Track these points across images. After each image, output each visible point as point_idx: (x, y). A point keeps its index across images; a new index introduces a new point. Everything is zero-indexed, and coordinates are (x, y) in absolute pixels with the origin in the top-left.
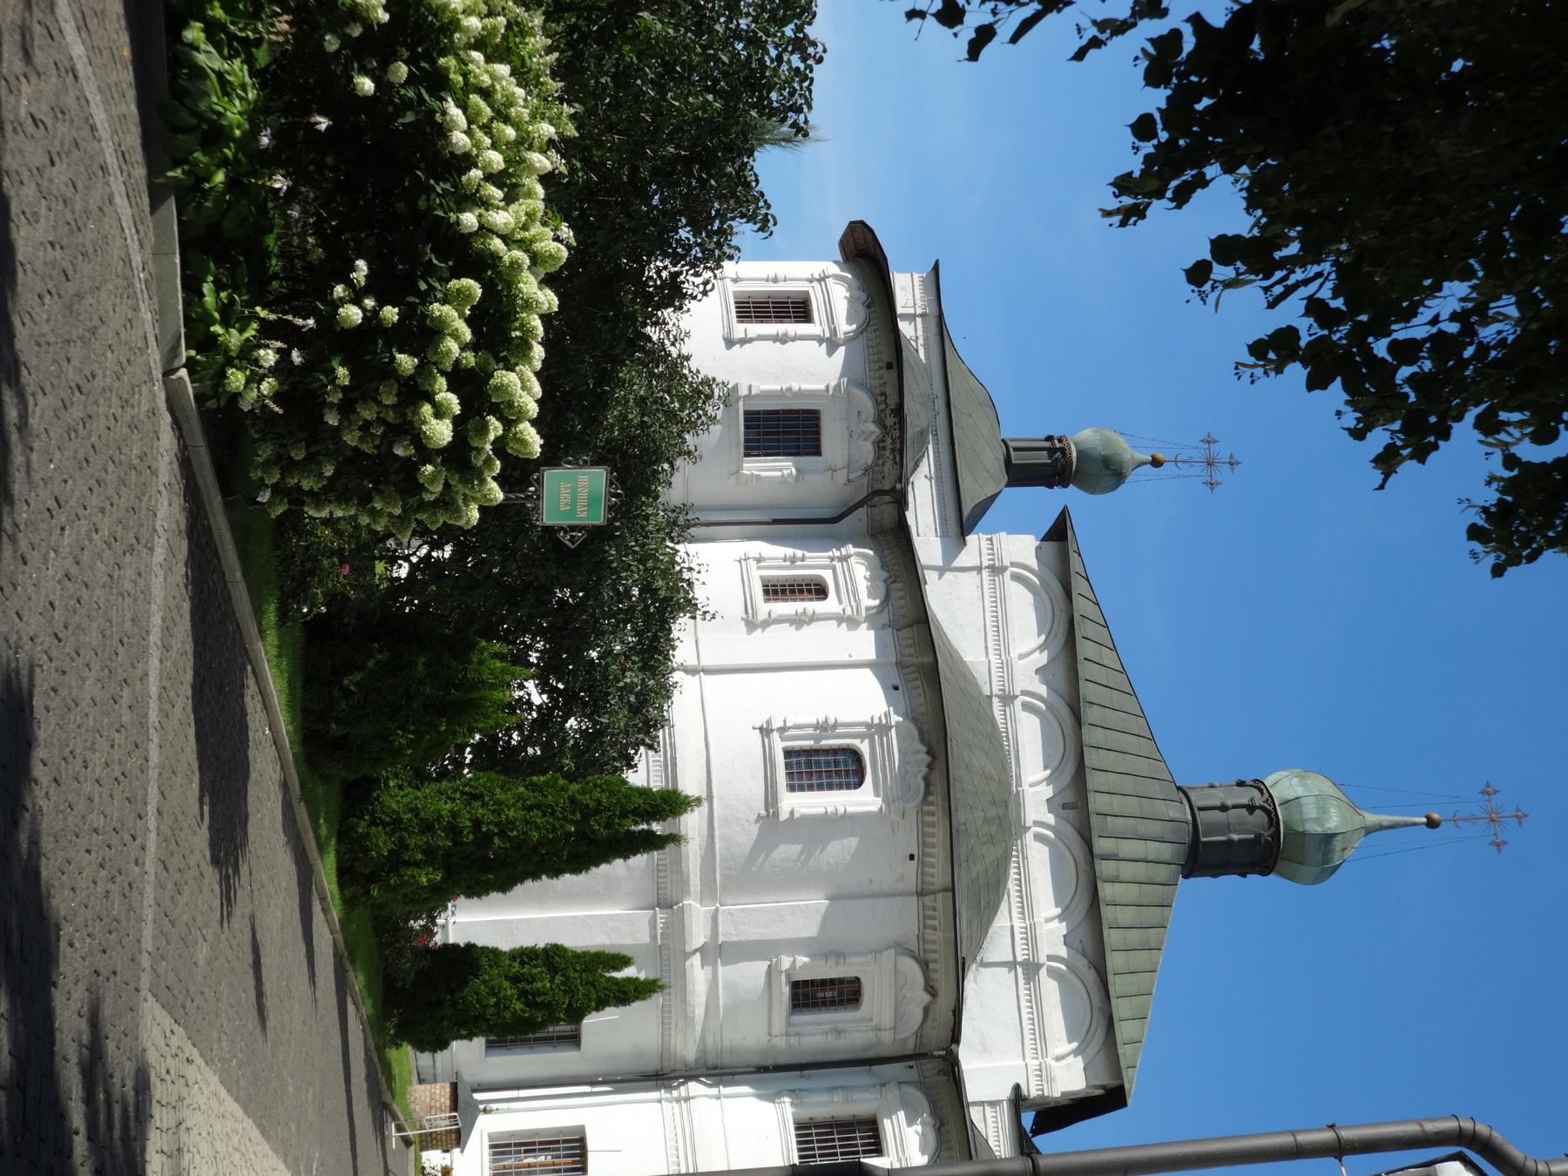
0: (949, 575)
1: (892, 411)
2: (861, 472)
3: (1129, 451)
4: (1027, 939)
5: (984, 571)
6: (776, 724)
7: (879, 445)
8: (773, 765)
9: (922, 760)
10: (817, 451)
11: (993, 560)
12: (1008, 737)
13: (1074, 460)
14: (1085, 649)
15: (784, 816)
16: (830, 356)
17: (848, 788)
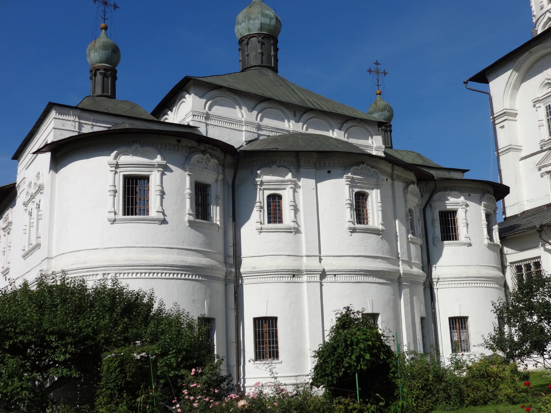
1: (199, 145)
3: (103, 38)
6: (259, 226)
16: (173, 171)
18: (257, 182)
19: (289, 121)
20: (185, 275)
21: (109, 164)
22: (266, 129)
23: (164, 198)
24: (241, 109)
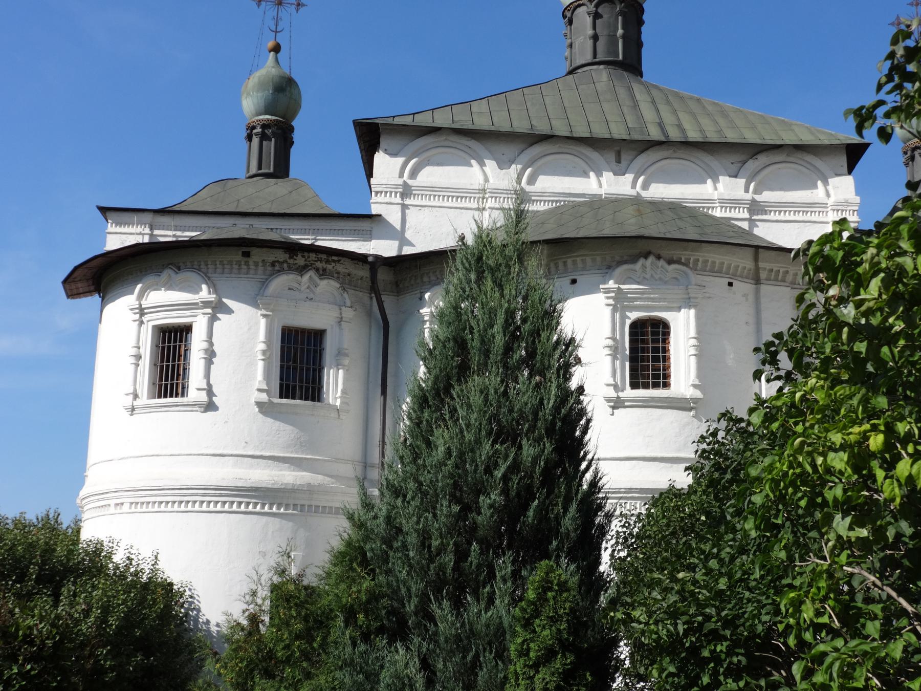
0: (408, 235)
1: (291, 258)
2: (346, 295)
3: (268, 68)
4: (731, 208)
5: (405, 203)
7: (323, 274)
8: (652, 399)
9: (652, 263)
10: (319, 335)
11: (396, 193)
12: (557, 201)
13: (274, 118)
14: (482, 123)
15: (698, 394)
16: (233, 312)
17: (668, 334)
18: (423, 317)
19: (599, 175)
20: (248, 504)
21: (131, 309)
22: (541, 198)
23: (213, 363)
24: (482, 164)
